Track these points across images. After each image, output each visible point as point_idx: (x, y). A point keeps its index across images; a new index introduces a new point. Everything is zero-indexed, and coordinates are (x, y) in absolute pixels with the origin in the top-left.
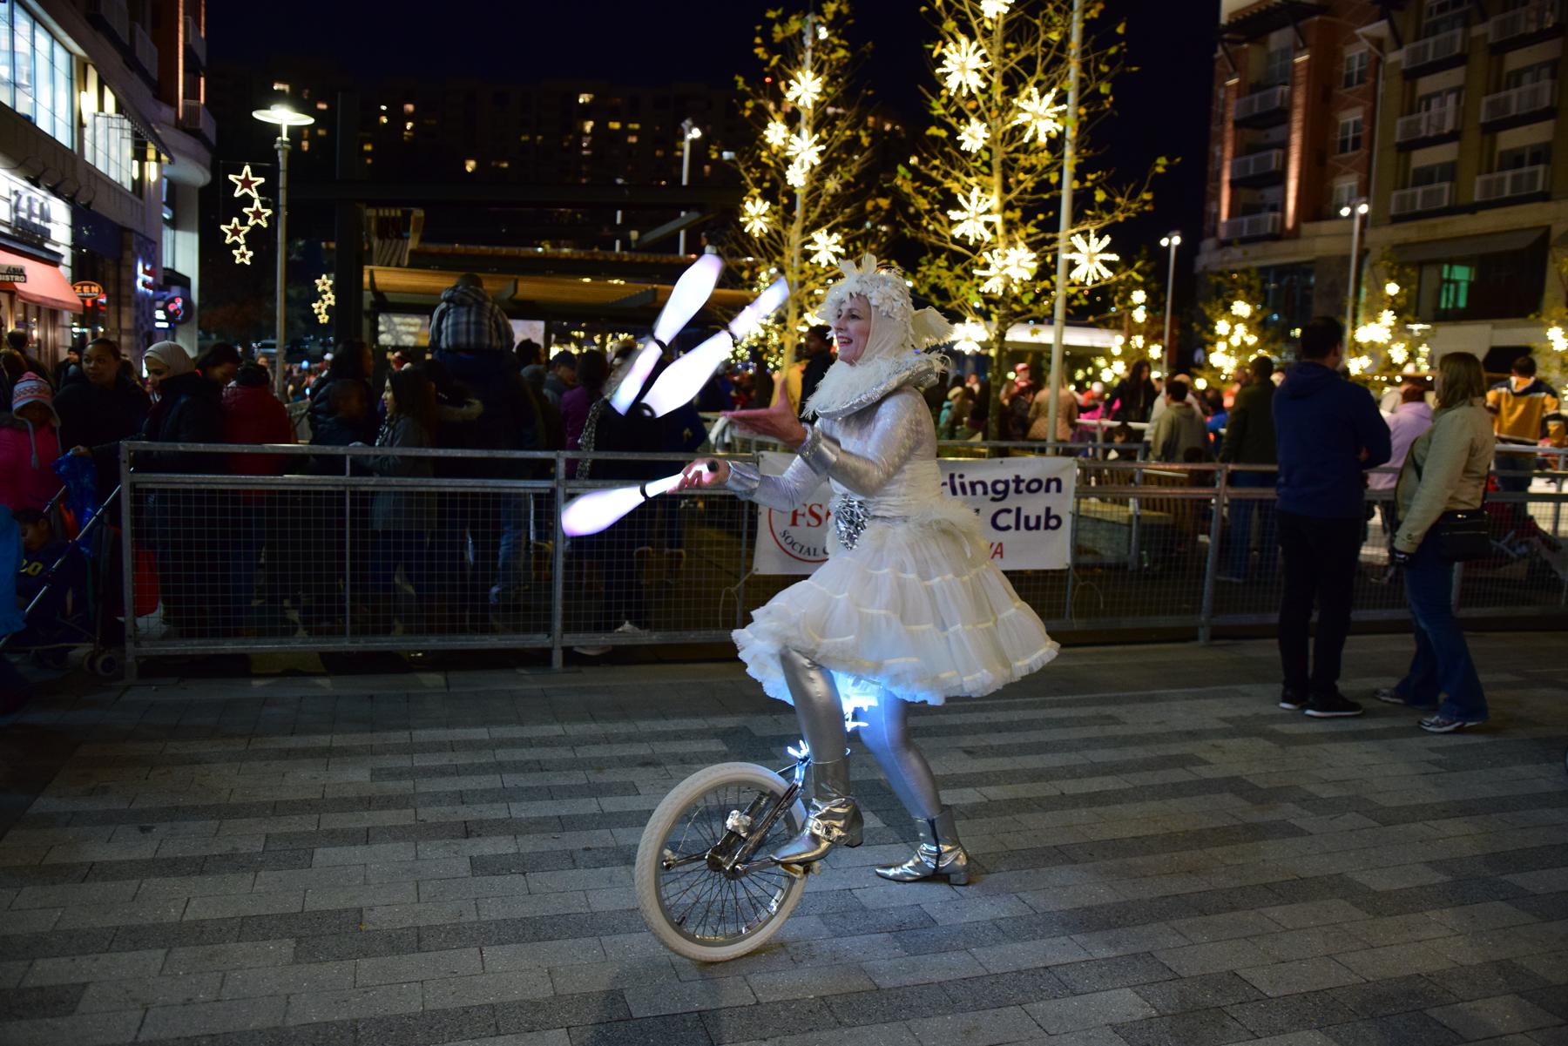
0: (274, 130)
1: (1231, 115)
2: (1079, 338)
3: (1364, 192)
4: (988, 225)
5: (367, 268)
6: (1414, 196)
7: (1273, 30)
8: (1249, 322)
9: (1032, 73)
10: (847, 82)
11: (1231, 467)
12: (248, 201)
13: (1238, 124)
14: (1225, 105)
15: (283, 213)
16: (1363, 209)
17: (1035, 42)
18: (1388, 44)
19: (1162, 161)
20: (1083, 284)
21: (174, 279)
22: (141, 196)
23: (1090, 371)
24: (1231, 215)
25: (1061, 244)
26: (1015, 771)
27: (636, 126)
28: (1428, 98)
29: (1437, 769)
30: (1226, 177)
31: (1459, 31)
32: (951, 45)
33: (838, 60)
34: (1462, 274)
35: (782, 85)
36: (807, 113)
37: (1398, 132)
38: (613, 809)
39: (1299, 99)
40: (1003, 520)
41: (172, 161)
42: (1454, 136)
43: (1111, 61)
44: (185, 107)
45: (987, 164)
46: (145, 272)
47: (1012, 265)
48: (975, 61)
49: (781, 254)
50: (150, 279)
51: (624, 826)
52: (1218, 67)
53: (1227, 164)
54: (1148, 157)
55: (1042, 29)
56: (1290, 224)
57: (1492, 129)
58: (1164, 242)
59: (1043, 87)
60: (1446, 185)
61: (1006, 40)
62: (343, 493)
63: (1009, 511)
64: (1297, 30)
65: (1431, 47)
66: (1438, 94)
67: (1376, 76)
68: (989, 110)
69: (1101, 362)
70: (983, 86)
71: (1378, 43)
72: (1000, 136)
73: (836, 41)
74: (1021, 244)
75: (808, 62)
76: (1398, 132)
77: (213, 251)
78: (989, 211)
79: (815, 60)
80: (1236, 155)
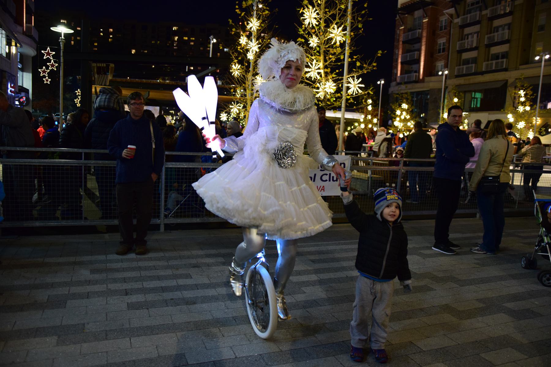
0: (59, 34)
1: (401, 39)
2: (349, 116)
3: (446, 67)
4: (319, 73)
5: (93, 87)
6: (463, 68)
7: (417, 10)
8: (407, 111)
9: (335, 19)
10: (269, 22)
11: (405, 159)
12: (49, 60)
13: (404, 42)
14: (399, 35)
15: (62, 64)
16: (446, 72)
17: (335, 9)
18: (455, 16)
19: (380, 52)
20: (352, 95)
21: (23, 90)
22: (9, 59)
23: (352, 127)
24: (401, 74)
25: (344, 81)
26: (329, 268)
27: (194, 39)
28: (468, 35)
29: (478, 266)
30: (400, 61)
31: (478, 13)
32: (306, 10)
33: (265, 14)
34: (479, 95)
35: (246, 24)
36: (254, 34)
37: (458, 47)
38: (182, 284)
39: (425, 34)
40: (324, 178)
41: (21, 46)
42: (476, 48)
43: (363, 16)
44: (26, 27)
45: (319, 52)
46: (11, 87)
47: (328, 87)
48: (314, 15)
49: (245, 83)
50: (13, 89)
51: (186, 290)
52: (397, 22)
53: (400, 56)
54: (374, 50)
55: (338, 4)
56: (421, 77)
57: (489, 46)
58: (379, 83)
59: (338, 25)
60: (474, 65)
61: (325, 8)
62: (81, 166)
63: (327, 175)
64: (424, 11)
65: (469, 18)
66: (471, 34)
67: (450, 27)
68: (319, 32)
69: (356, 124)
70: (317, 24)
71: (451, 16)
72: (323, 42)
73: (265, 8)
74: (330, 80)
75: (255, 15)
76: (458, 47)
77: (37, 80)
78: (319, 69)
79: (257, 14)
80: (403, 53)
